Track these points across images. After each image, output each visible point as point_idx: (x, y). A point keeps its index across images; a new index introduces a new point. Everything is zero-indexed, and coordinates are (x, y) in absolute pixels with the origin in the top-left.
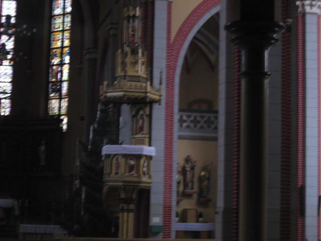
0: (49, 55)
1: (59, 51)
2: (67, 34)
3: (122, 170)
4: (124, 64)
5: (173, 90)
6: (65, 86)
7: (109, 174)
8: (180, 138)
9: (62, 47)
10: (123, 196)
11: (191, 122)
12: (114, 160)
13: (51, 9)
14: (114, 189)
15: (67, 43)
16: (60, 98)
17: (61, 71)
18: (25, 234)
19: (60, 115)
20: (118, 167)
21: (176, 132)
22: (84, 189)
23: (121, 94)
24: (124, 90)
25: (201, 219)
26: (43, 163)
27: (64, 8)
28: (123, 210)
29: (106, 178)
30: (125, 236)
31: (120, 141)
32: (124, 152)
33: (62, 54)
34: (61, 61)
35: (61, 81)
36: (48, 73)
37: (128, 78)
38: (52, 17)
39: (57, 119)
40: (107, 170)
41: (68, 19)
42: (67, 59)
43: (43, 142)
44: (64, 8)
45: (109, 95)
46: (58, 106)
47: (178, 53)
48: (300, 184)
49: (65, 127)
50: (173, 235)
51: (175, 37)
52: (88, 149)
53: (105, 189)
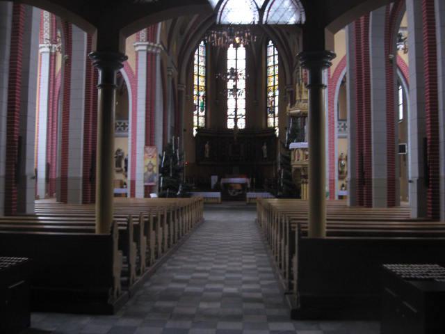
0: (267, 91)
1: (272, 88)
2: (277, 77)
3: (301, 158)
4: (300, 92)
5: (333, 107)
6: (277, 110)
7: (294, 160)
8: (339, 137)
9: (274, 86)
10: (303, 174)
11: (342, 127)
12: (297, 152)
13: (266, 63)
14: (298, 170)
15: (277, 83)
16: (274, 117)
17: (274, 101)
18: (250, 198)
19: (274, 127)
20: (299, 156)
21: (336, 135)
22: (282, 171)
23: (298, 111)
24: (407, 95)
25: (344, 188)
26: (265, 156)
27: (274, 62)
28: (303, 182)
29: (292, 163)
30: (409, 206)
31: (148, 149)
32: (302, 147)
33: (274, 89)
34: (274, 94)
35: (274, 107)
36: (267, 102)
37: (302, 101)
38: (267, 67)
39: (273, 129)
40: (292, 158)
41: (277, 68)
42: (277, 93)
43: (265, 144)
44: (274, 62)
45: (291, 112)
46: (272, 122)
47: (336, 84)
48: (35, 167)
49: (278, 134)
50: (336, 198)
51: (335, 72)
52: (267, 145)
53: (293, 170)
